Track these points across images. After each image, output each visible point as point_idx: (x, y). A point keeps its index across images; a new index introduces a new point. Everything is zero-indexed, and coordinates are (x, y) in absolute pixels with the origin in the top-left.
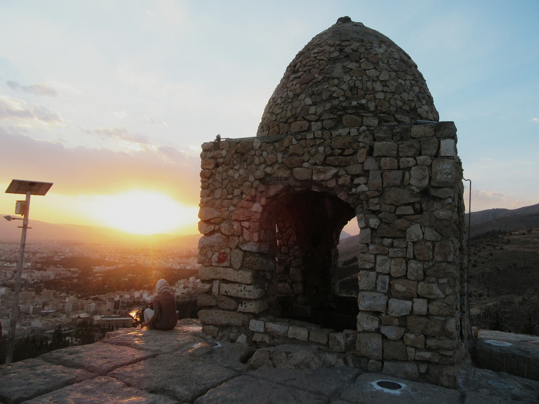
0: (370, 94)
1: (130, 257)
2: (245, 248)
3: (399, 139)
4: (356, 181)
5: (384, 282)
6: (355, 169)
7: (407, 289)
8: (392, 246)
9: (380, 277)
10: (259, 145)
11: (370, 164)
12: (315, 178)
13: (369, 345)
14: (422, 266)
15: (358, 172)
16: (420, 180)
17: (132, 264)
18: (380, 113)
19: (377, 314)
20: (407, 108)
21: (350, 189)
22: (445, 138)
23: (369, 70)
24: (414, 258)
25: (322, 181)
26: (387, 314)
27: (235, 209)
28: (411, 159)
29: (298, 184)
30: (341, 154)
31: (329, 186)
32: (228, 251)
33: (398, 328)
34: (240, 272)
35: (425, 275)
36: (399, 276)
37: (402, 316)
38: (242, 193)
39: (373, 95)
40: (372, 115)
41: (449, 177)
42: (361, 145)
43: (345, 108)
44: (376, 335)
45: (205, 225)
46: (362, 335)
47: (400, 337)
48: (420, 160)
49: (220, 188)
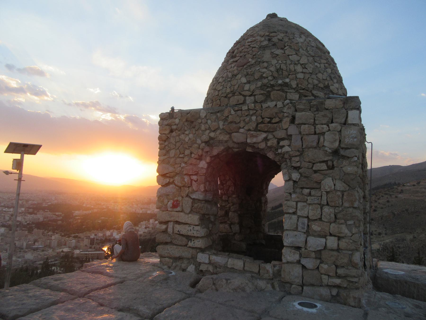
0: (293, 74)
2: (194, 196)
3: (315, 110)
4: (281, 143)
5: (303, 224)
6: (280, 134)
8: (310, 194)
10: (204, 115)
11: (292, 130)
12: (249, 141)
13: (292, 273)
15: (283, 137)
17: (104, 209)
18: (300, 90)
19: (298, 248)
20: (321, 85)
21: (277, 150)
24: (328, 204)
25: (255, 143)
26: (306, 249)
27: (186, 165)
30: (269, 122)
31: (260, 147)
34: (190, 215)
35: (336, 217)
36: (315, 218)
39: (295, 76)
40: (294, 91)
41: (355, 140)
42: (286, 115)
43: (272, 86)
44: (298, 265)
45: (162, 178)
46: (286, 265)
47: (316, 267)
49: (174, 149)
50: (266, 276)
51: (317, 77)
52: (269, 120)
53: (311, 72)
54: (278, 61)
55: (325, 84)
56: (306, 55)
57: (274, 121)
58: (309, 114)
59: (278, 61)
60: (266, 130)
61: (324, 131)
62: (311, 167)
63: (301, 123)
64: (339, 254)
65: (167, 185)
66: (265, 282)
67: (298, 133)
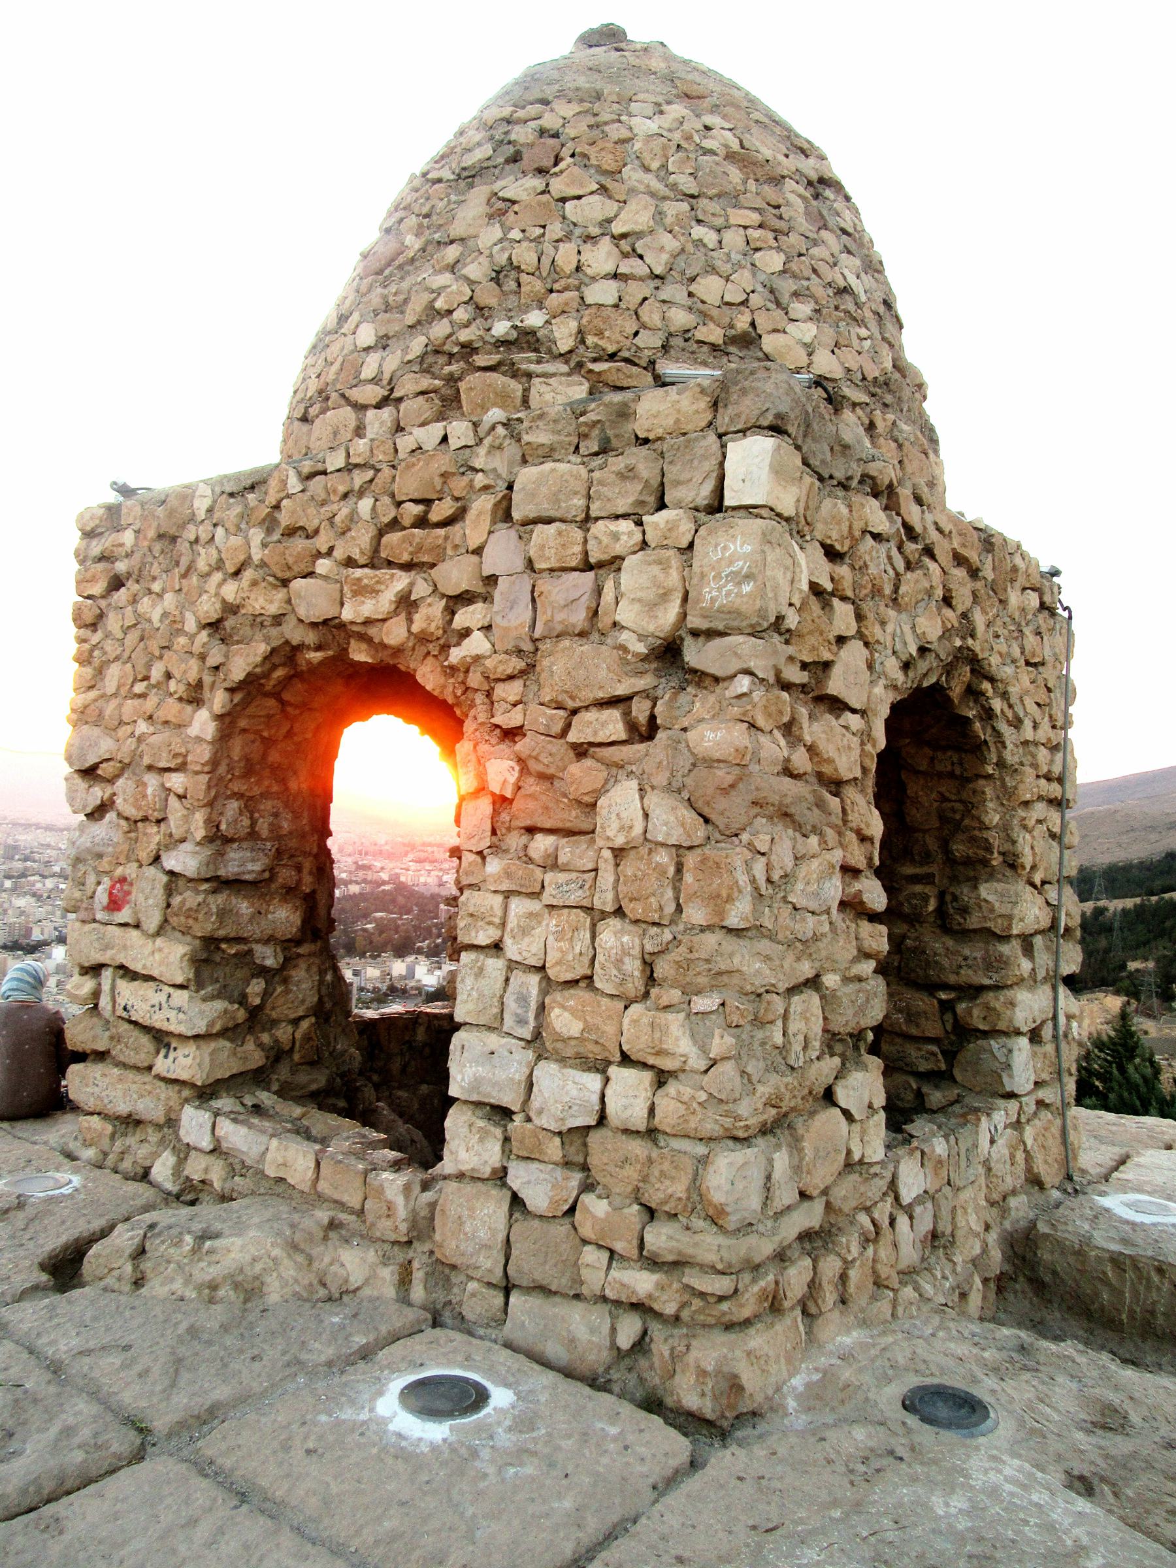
0: (567, 288)
1: (378, 864)
2: (171, 862)
3: (596, 449)
4: (462, 618)
5: (523, 999)
6: (456, 574)
7: (587, 1029)
8: (552, 864)
9: (518, 978)
10: (207, 502)
11: (503, 553)
12: (347, 614)
13: (468, 1228)
14: (637, 941)
15: (464, 587)
16: (652, 607)
17: (384, 883)
18: (595, 360)
19: (502, 1113)
20: (715, 335)
21: (445, 648)
23: (579, 197)
24: (619, 912)
25: (368, 622)
26: (529, 1119)
27: (152, 729)
28: (626, 526)
29: (311, 638)
30: (422, 522)
31: (386, 641)
32: (130, 870)
33: (559, 1173)
34: (159, 941)
35: (651, 979)
36: (569, 976)
37: (570, 1130)
38: (168, 676)
39: (574, 294)
40: (565, 368)
41: (747, 588)
42: (480, 480)
43: (469, 349)
44: (494, 1192)
45: (81, 784)
46: (453, 1185)
47: (566, 1207)
48: (656, 525)
49: (117, 659)
50: (384, 1228)
51: (690, 295)
52: (418, 509)
53: (658, 271)
54: (506, 229)
55: (731, 326)
56: (653, 194)
57: (434, 517)
58: (568, 469)
59: (506, 229)
60: (405, 557)
61: (618, 549)
62: (557, 728)
63: (532, 515)
64: (655, 1154)
65: (97, 813)
66: (371, 1256)
67: (520, 565)
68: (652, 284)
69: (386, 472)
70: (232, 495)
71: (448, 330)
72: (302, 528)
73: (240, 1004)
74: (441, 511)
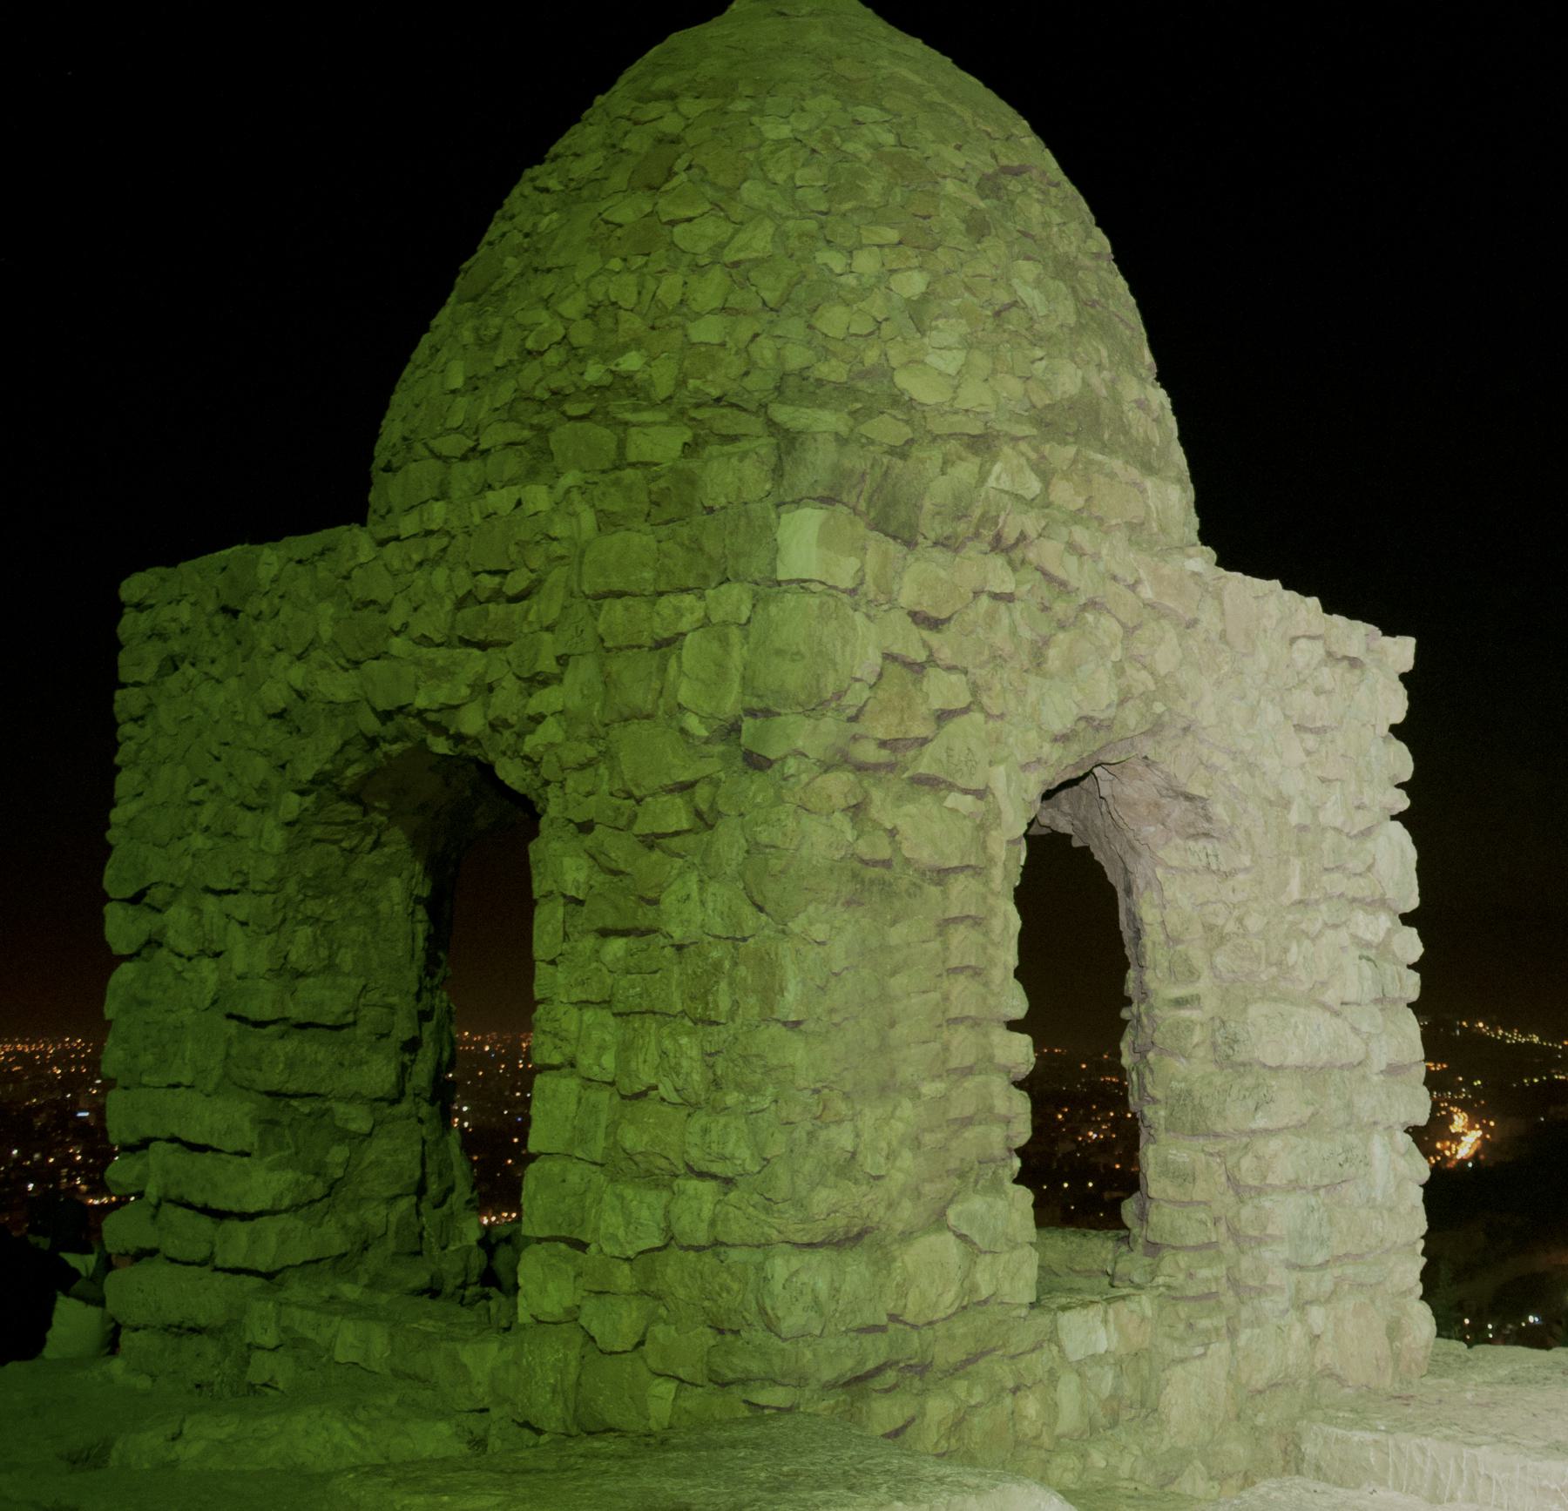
9: (593, 1096)
18: (698, 406)
22: (774, 570)
23: (690, 220)
68: (768, 316)
69: (460, 538)
70: (300, 562)
71: (539, 374)
72: (373, 602)
73: (317, 1174)
74: (517, 582)
